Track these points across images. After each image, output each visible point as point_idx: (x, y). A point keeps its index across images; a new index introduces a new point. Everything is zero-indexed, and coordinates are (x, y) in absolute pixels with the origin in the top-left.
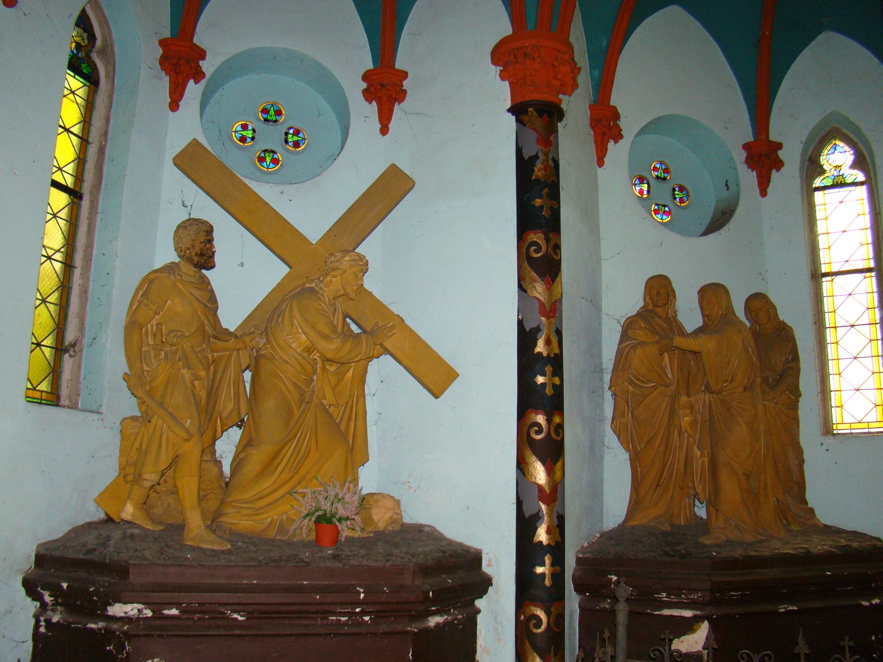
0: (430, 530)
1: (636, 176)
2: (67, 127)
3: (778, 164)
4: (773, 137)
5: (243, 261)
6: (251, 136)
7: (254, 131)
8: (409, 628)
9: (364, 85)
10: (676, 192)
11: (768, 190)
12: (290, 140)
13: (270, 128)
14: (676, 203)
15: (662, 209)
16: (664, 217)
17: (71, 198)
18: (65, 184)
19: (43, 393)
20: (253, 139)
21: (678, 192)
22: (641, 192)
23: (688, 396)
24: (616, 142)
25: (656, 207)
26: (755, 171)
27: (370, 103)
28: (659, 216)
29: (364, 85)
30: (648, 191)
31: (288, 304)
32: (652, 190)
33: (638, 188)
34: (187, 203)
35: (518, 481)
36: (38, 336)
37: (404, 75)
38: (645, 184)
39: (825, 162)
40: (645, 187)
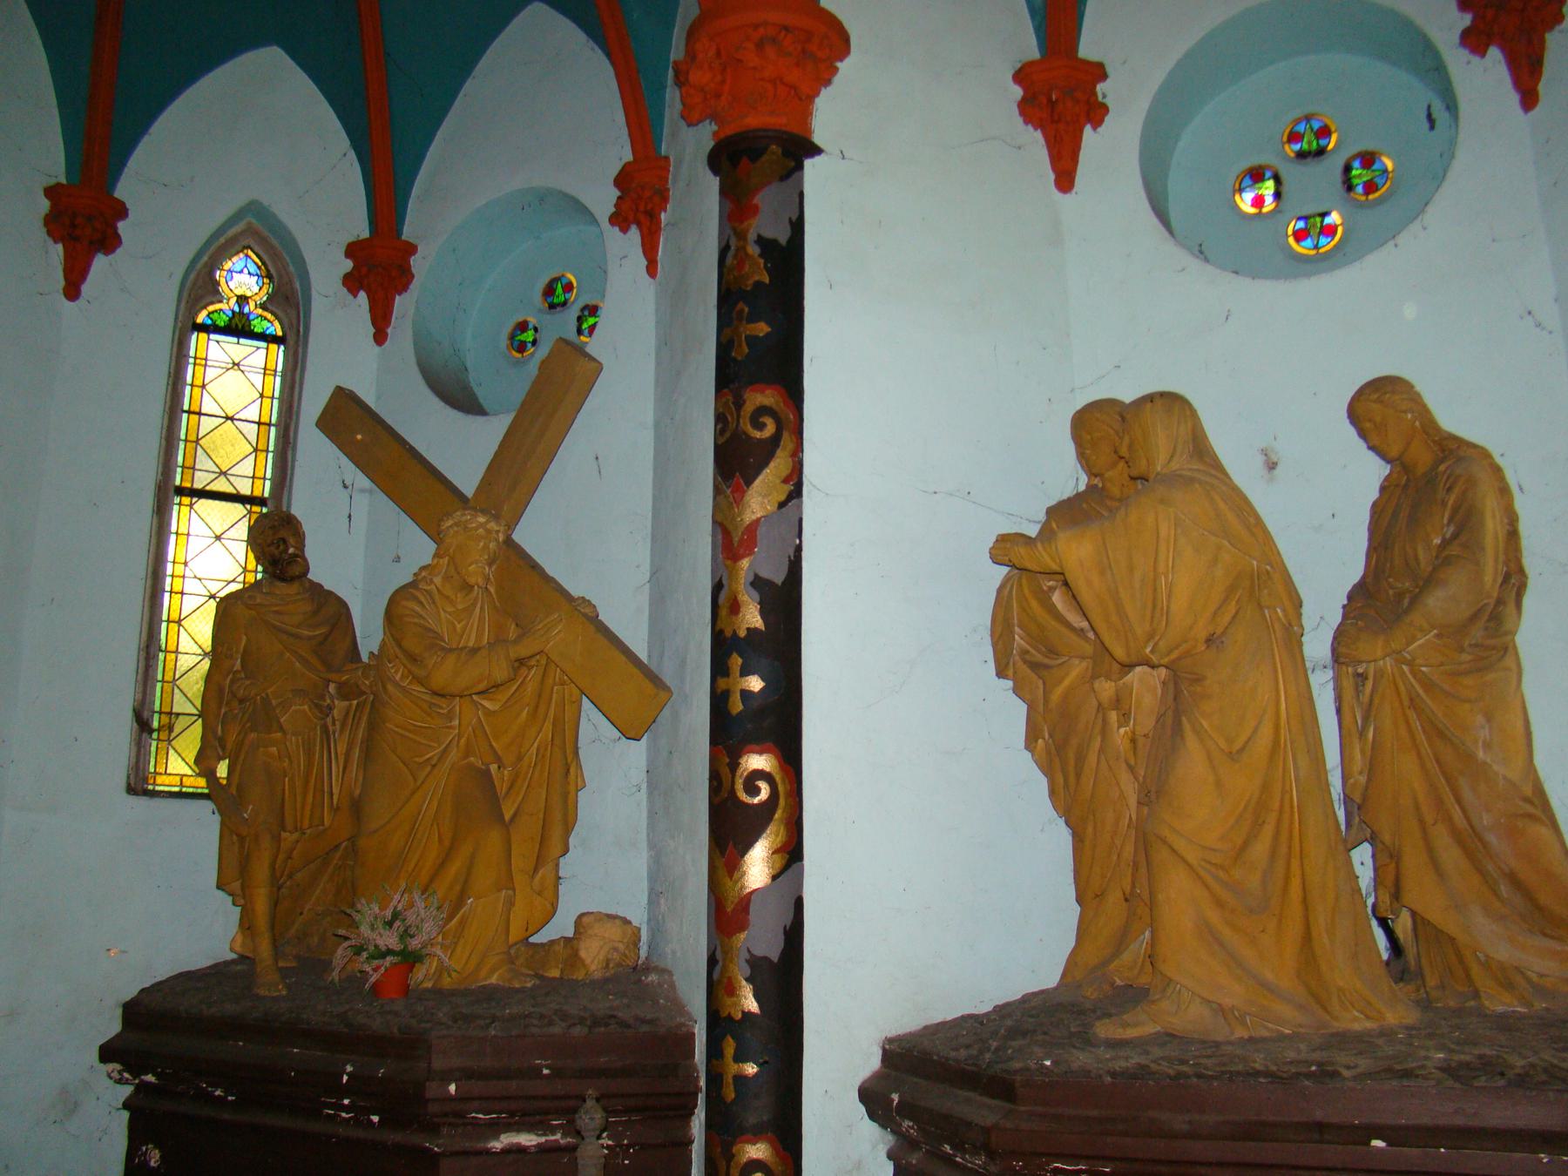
0: (656, 981)
1: (573, 302)
2: (229, 422)
3: (1096, 113)
4: (1088, 49)
5: (400, 555)
6: (531, 339)
7: (536, 330)
8: (427, 1145)
9: (348, 265)
10: (1354, 172)
11: (1541, 88)
12: (1355, 181)
13: (1313, 168)
14: (1356, 199)
15: (1314, 225)
16: (1323, 241)
17: (246, 508)
18: (235, 492)
19: (163, 771)
20: (534, 343)
21: (1359, 172)
22: (1258, 201)
23: (284, 767)
24: (1095, 128)
25: (1301, 225)
26: (362, 295)
27: (355, 296)
28: (1308, 243)
29: (348, 265)
30: (1277, 195)
31: (482, 608)
32: (1285, 189)
33: (1248, 196)
34: (348, 482)
35: (756, 892)
36: (185, 702)
37: (1098, 72)
38: (1269, 179)
39: (223, 281)
40: (1268, 188)
